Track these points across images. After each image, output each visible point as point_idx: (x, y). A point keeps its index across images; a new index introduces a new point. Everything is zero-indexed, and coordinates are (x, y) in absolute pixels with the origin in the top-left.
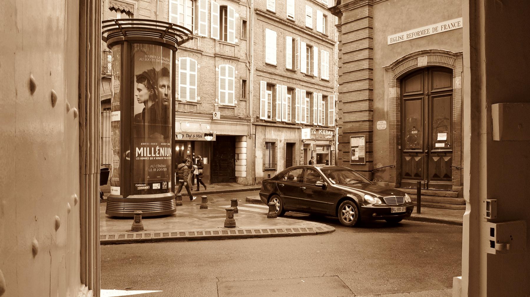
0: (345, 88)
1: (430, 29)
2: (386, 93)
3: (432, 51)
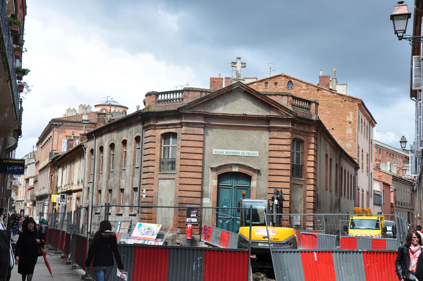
1: (241, 153)
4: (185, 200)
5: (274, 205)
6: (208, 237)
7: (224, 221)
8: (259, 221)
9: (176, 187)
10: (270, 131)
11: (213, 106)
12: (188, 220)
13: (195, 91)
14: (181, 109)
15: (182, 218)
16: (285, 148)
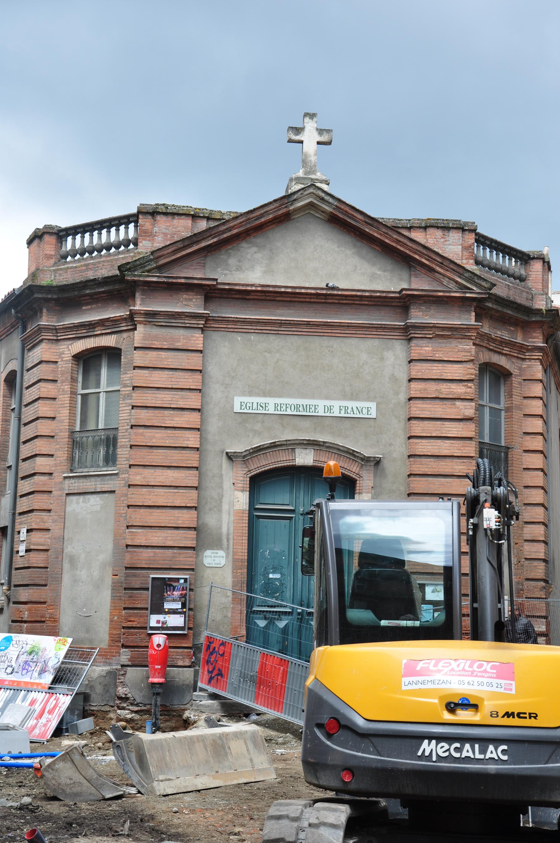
0: (138, 477)
1: (320, 406)
2: (225, 501)
3: (327, 445)
4: (145, 557)
5: (480, 536)
6: (220, 674)
7: (271, 622)
8: (412, 613)
9: (118, 515)
10: (410, 340)
11: (232, 261)
12: (154, 620)
13: (173, 214)
14: (129, 270)
15: (136, 615)
16: (459, 390)
